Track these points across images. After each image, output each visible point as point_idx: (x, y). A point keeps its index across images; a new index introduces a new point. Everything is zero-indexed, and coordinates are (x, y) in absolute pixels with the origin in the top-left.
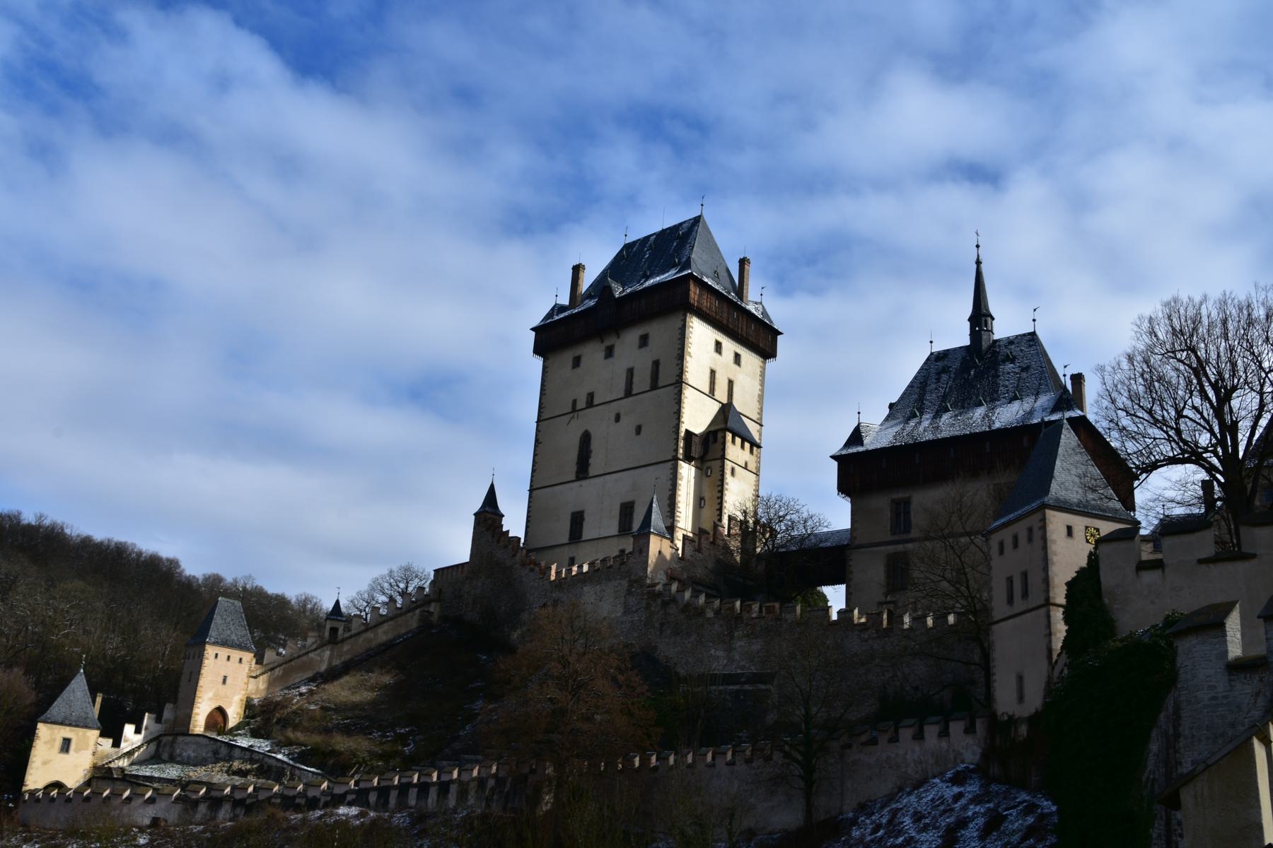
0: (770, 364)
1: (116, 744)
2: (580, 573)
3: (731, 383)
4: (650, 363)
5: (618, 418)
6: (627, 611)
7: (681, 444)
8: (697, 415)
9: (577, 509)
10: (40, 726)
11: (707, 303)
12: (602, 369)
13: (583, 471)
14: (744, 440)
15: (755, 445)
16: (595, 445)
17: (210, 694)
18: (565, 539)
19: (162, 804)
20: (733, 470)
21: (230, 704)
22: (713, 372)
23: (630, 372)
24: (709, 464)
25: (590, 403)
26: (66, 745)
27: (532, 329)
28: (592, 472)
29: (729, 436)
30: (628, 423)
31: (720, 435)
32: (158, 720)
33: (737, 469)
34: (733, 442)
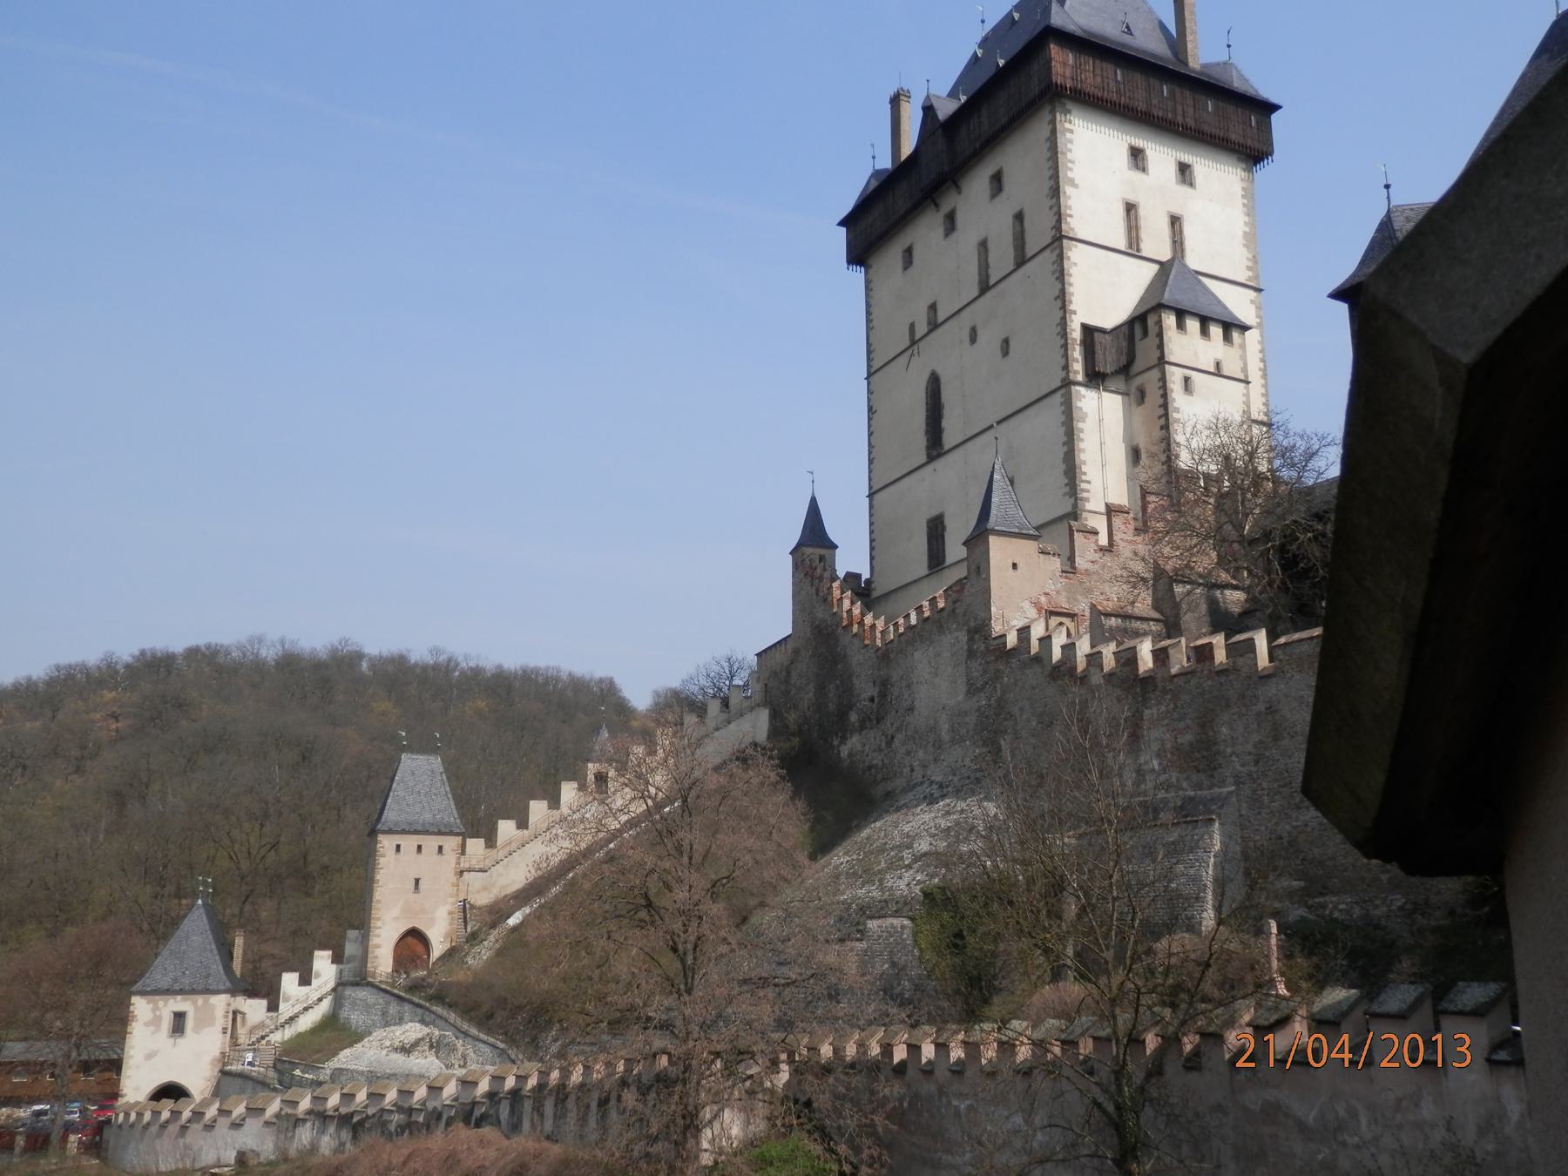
0: (1265, 171)
1: (273, 1007)
2: (910, 628)
3: (1175, 221)
4: (1010, 220)
5: (973, 338)
6: (972, 690)
7: (1077, 353)
8: (1103, 292)
9: (934, 513)
10: (135, 1000)
11: (1092, 75)
12: (939, 254)
13: (935, 445)
14: (1205, 321)
16: (947, 395)
17: (396, 912)
18: (924, 571)
19: (253, 1125)
20: (1187, 379)
21: (432, 921)
22: (1130, 208)
23: (983, 245)
24: (1137, 381)
25: (934, 326)
28: (949, 440)
29: (1170, 320)
30: (989, 339)
31: (1151, 320)
32: (337, 959)
34: (1181, 326)
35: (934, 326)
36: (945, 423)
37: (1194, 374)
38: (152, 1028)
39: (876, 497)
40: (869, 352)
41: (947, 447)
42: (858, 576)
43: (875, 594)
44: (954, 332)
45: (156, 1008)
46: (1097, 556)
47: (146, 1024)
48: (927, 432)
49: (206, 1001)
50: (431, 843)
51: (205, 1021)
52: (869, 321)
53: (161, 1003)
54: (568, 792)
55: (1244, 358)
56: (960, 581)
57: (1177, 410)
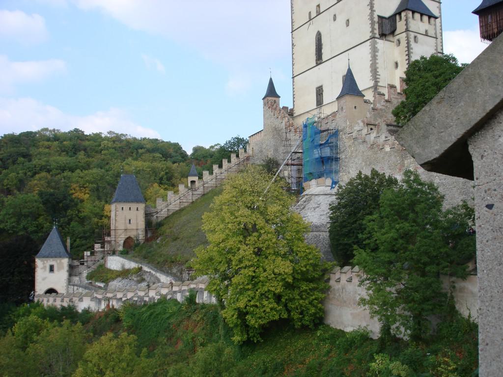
15: (431, 16)
18: (315, 107)
24: (397, 37)
26: (52, 269)
27: (475, 12)
28: (324, 58)
30: (341, 19)
33: (419, 36)
35: (319, 13)
36: (323, 51)
37: (419, 36)
38: (43, 270)
39: (295, 78)
40: (292, 23)
41: (324, 61)
42: (287, 108)
43: (295, 115)
44: (328, 16)
45: (44, 263)
46: (384, 104)
47: (42, 269)
48: (316, 54)
49: (60, 261)
50: (134, 206)
51: (60, 269)
52: (292, 10)
53: (45, 262)
54: (181, 188)
55: (435, 29)
56: (334, 113)
57: (412, 49)
